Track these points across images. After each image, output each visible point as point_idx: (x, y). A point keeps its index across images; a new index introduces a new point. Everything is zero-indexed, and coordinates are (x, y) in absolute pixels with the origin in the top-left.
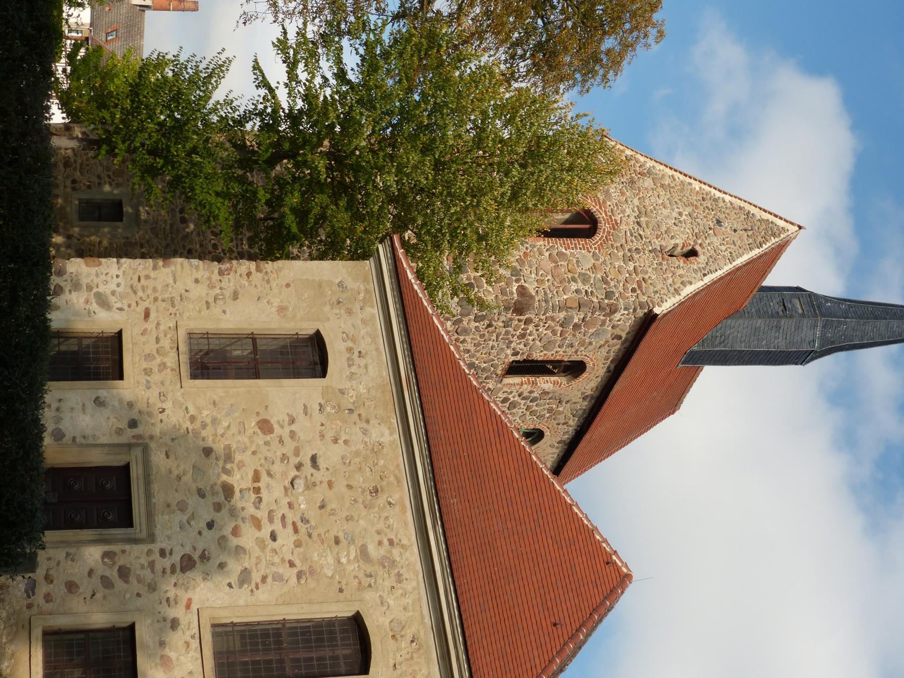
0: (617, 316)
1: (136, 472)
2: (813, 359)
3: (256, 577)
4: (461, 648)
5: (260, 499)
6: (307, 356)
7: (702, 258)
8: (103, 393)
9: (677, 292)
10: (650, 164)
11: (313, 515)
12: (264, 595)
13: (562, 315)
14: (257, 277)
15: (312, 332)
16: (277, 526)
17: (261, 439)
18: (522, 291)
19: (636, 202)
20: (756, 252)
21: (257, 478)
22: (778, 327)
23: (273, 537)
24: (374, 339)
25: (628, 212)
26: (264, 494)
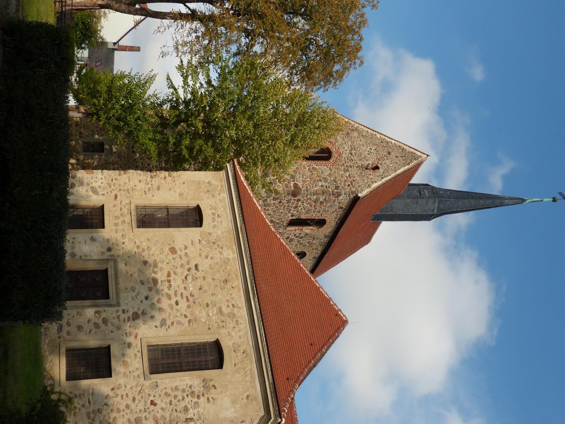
0: (341, 198)
1: (111, 273)
3: (169, 322)
4: (267, 356)
6: (193, 217)
7: (381, 170)
8: (95, 235)
9: (369, 186)
10: (356, 125)
11: (196, 293)
12: (172, 331)
13: (315, 197)
14: (169, 179)
15: (195, 205)
16: (179, 298)
18: (296, 186)
19: (350, 143)
20: (407, 167)
21: (169, 275)
22: (417, 203)
23: (177, 303)
24: (225, 209)
25: (346, 148)
26: (172, 283)
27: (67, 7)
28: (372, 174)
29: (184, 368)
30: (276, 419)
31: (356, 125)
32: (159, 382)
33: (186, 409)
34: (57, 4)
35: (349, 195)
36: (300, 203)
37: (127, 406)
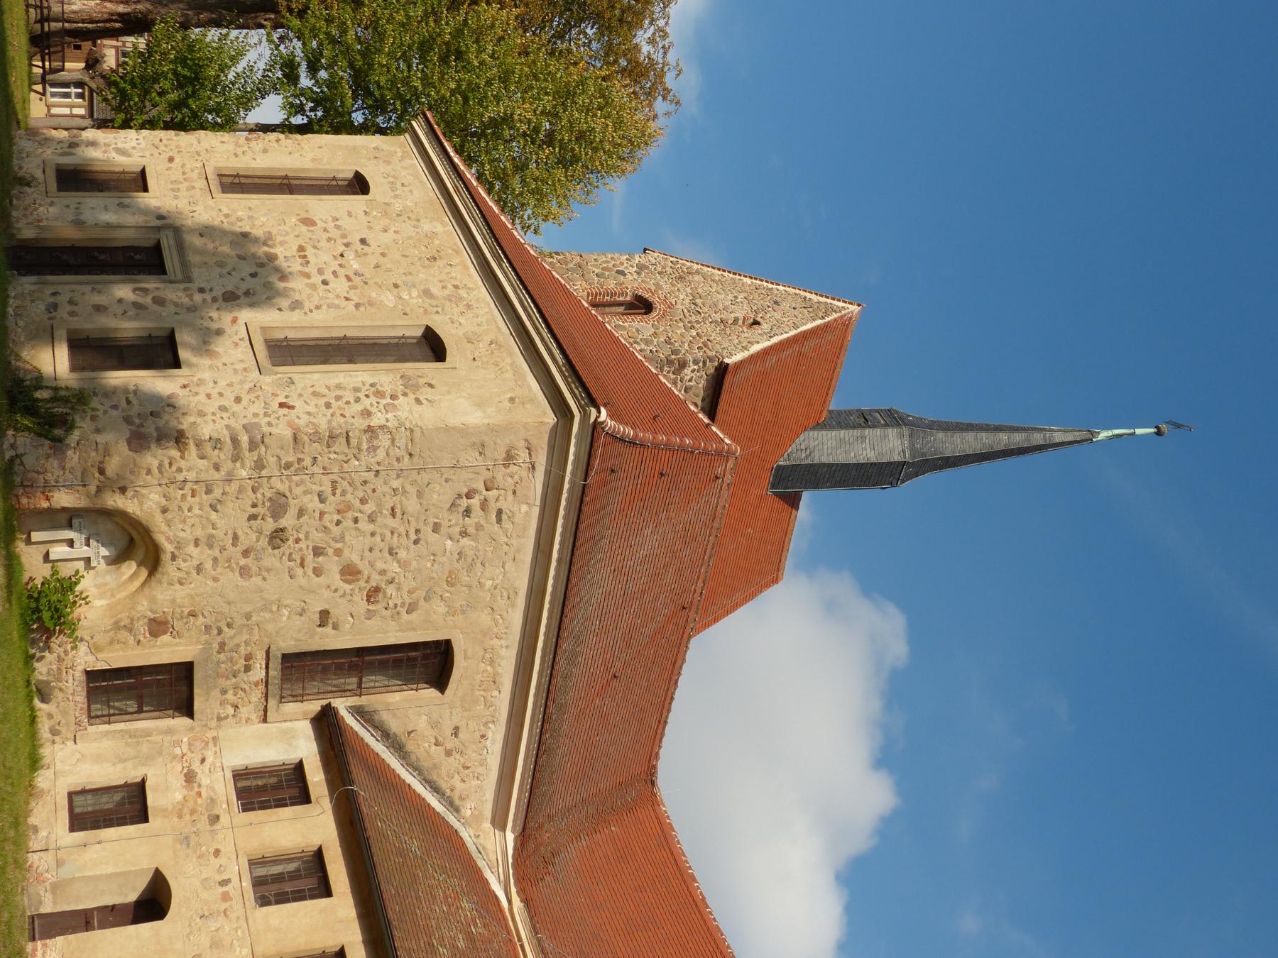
0: (687, 371)
2: (909, 477)
4: (544, 332)
8: (126, 201)
9: (745, 348)
10: (695, 267)
15: (350, 175)
16: (328, 276)
19: (689, 290)
20: (819, 322)
21: (301, 248)
22: (863, 438)
24: (416, 177)
25: (681, 297)
26: (311, 259)
27: (53, 24)
28: (747, 334)
30: (585, 415)
32: (296, 377)
33: (367, 413)
34: (32, 10)
35: (704, 363)
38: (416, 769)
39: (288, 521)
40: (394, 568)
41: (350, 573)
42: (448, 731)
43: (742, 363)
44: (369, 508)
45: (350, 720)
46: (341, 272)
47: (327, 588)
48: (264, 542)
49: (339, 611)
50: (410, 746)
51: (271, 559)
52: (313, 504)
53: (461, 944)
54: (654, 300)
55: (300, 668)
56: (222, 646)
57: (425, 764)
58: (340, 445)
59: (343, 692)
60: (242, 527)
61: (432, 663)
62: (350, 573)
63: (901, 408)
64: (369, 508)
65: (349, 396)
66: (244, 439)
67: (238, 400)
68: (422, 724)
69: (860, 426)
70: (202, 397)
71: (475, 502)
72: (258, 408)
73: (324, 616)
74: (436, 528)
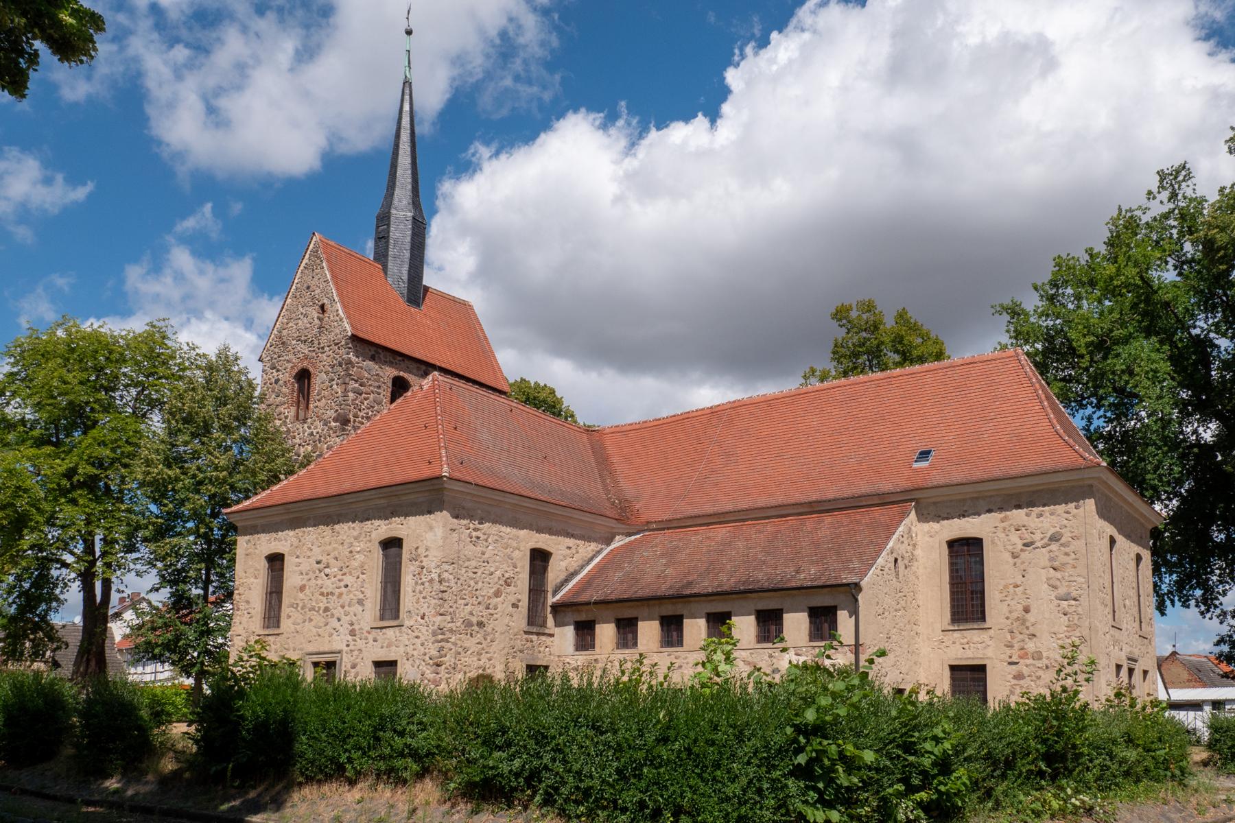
1: (316, 659)
3: (361, 596)
5: (157, 590)
6: (276, 561)
7: (325, 301)
10: (275, 331)
11: (340, 564)
12: (368, 593)
13: (351, 395)
14: (241, 590)
16: (342, 584)
17: (307, 591)
18: (335, 420)
21: (322, 594)
22: (396, 241)
23: (346, 586)
26: (329, 590)
28: (330, 314)
29: (979, 589)
31: (275, 331)
33: (431, 581)
36: (361, 414)
37: (422, 645)
38: (582, 567)
39: (474, 620)
40: (498, 573)
41: (497, 594)
42: (569, 551)
43: (352, 325)
44: (472, 583)
45: (558, 597)
46: (339, 577)
47: (503, 604)
48: (481, 631)
49: (512, 599)
50: (572, 570)
51: (488, 629)
52: (469, 608)
53: (664, 561)
54: (300, 366)
55: (534, 619)
56: (521, 651)
57: (580, 563)
58: (445, 596)
59: (545, 598)
60: (474, 640)
61: (540, 558)
62: (497, 594)
63: (377, 211)
64: (472, 583)
65: (420, 588)
66: (440, 637)
67: (417, 637)
68: (563, 564)
69: (387, 242)
70: (415, 653)
71: (474, 534)
72: (424, 629)
73: (515, 606)
74: (483, 554)
